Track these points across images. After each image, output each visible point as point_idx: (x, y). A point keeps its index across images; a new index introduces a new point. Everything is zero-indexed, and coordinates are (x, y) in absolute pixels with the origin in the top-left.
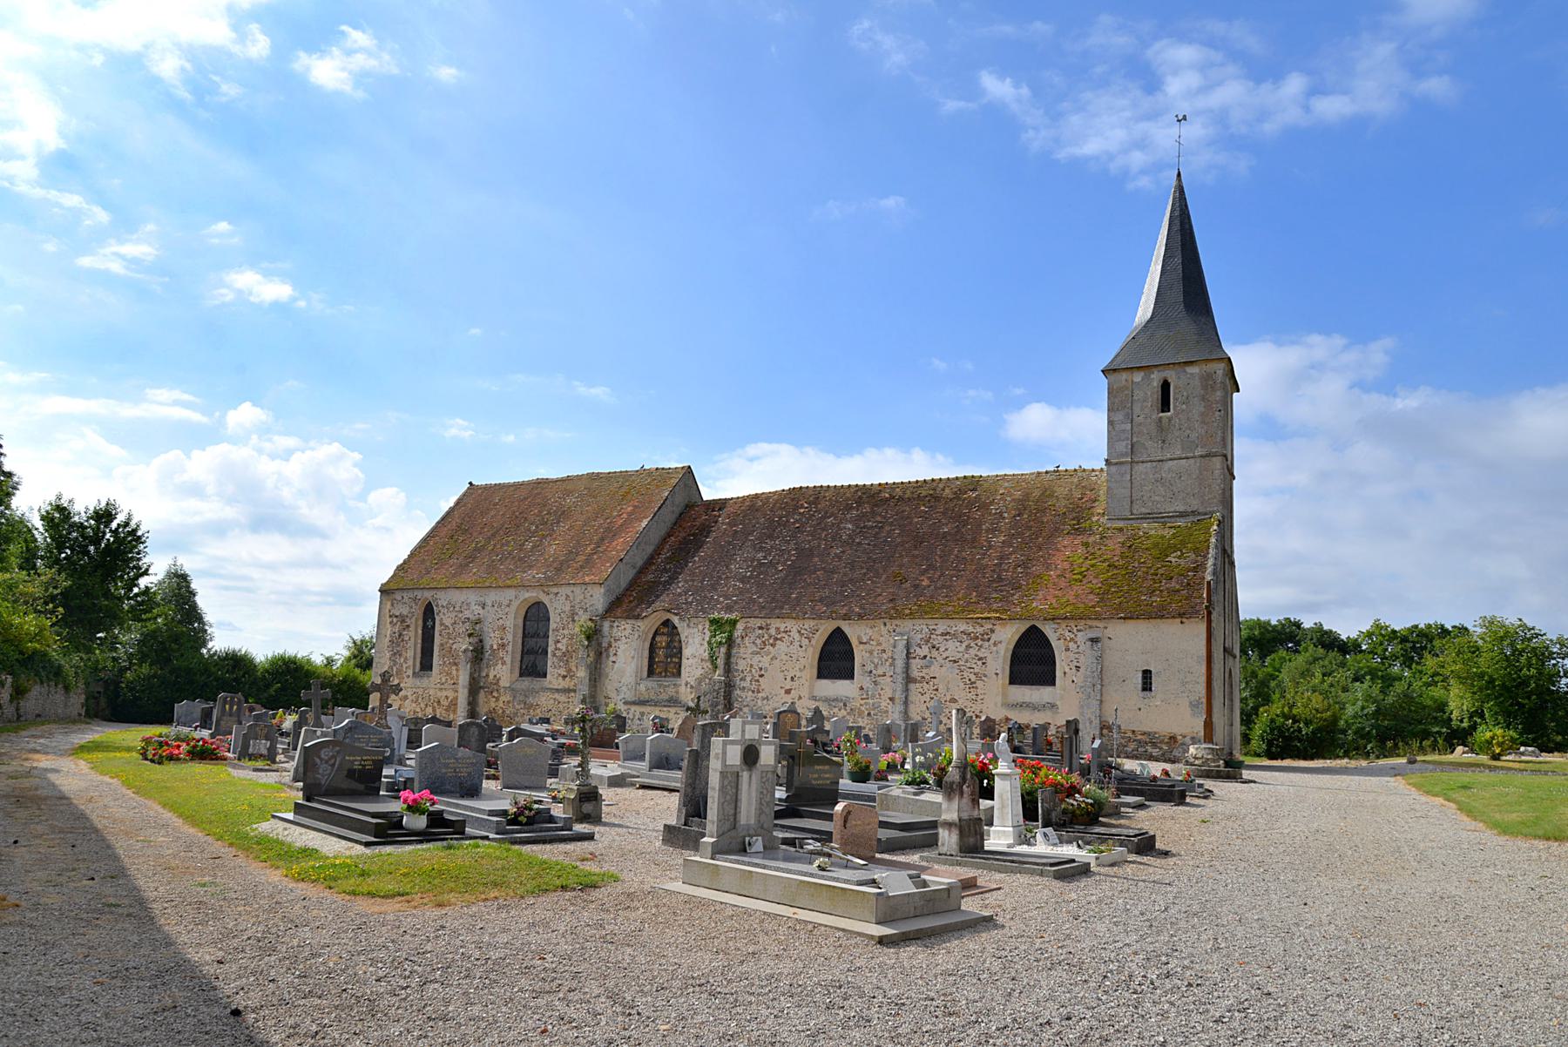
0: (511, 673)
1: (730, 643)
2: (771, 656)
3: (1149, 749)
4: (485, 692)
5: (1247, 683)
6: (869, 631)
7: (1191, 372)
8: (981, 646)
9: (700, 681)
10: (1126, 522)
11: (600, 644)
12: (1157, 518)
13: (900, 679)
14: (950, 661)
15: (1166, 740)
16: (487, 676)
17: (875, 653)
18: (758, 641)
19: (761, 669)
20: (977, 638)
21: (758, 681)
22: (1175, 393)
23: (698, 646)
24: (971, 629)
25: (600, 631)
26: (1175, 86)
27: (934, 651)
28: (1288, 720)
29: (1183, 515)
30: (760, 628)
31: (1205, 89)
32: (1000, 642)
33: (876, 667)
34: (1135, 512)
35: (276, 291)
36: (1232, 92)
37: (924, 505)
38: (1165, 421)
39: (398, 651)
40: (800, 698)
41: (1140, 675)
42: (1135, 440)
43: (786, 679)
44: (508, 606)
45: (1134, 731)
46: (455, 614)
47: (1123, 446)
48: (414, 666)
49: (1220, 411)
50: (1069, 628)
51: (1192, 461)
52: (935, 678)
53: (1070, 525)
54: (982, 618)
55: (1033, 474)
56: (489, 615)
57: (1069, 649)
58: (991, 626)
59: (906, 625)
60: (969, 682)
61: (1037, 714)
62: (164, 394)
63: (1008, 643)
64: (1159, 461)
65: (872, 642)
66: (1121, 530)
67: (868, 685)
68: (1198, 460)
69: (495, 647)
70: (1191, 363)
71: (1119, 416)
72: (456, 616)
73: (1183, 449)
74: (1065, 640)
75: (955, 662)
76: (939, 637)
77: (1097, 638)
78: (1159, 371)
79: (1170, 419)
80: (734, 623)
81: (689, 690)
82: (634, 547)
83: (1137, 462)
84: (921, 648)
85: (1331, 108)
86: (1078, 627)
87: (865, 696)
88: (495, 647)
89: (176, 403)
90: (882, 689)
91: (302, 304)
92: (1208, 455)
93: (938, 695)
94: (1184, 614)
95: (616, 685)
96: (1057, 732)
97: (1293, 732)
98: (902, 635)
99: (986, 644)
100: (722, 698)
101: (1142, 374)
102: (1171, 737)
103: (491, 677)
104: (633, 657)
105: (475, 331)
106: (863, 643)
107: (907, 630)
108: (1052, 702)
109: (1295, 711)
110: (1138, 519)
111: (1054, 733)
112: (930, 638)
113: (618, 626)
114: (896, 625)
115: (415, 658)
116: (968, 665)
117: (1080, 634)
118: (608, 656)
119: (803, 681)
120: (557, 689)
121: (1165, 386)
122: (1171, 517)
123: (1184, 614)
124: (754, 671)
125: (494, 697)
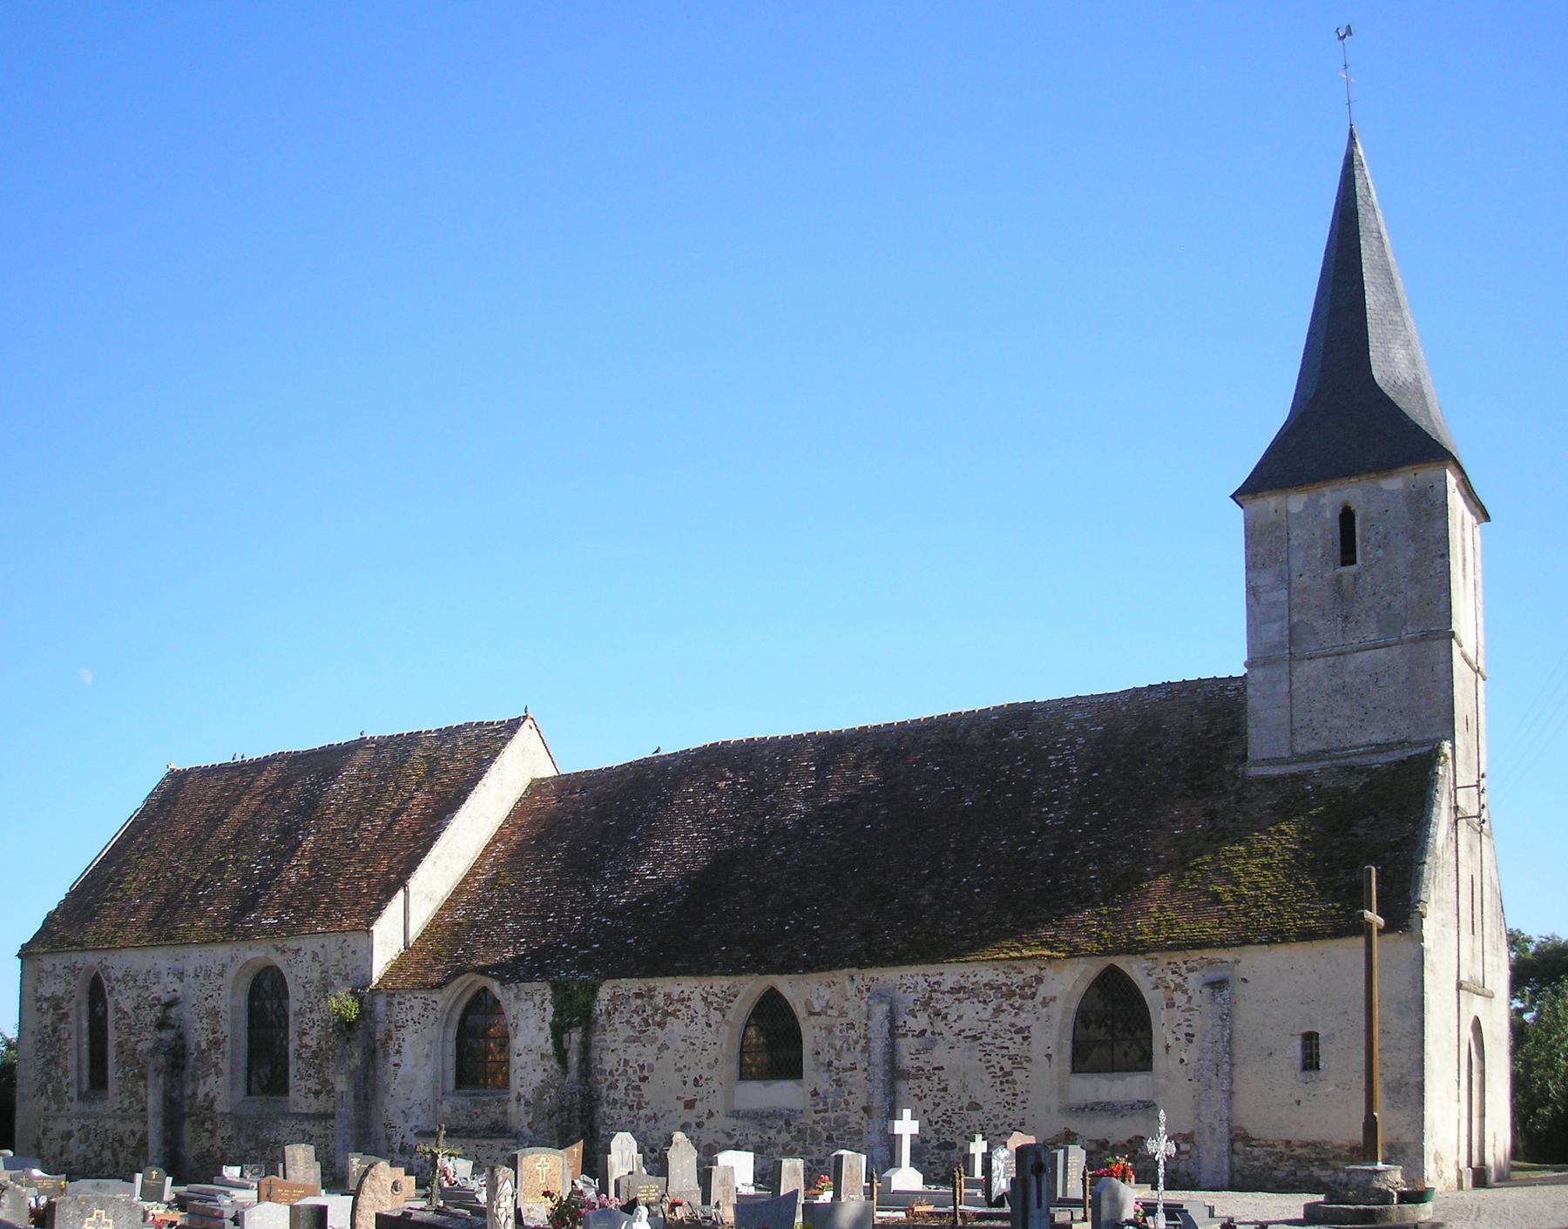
4: (193, 1122)
6: (826, 993)
13: (879, 1073)
15: (1345, 1153)
17: (837, 1030)
20: (1011, 994)
24: (1002, 979)
25: (371, 1012)
30: (638, 996)
32: (1054, 999)
33: (838, 1055)
40: (711, 1114)
41: (1298, 1042)
42: (1295, 619)
43: (685, 1083)
44: (221, 975)
45: (1288, 1143)
48: (79, 1082)
50: (1172, 966)
52: (941, 1068)
57: (1173, 1005)
64: (1338, 655)
65: (830, 1012)
69: (204, 1046)
72: (139, 996)
73: (1380, 630)
75: (975, 1038)
76: (947, 996)
79: (1356, 577)
87: (821, 1107)
88: (204, 1046)
90: (850, 1093)
93: (948, 1098)
99: (1029, 1003)
103: (201, 1097)
104: (428, 1056)
108: (1145, 1099)
112: (931, 998)
115: (79, 1068)
116: (998, 1042)
117: (1191, 976)
118: (386, 1056)
119: (714, 1085)
122: (1362, 754)
124: (630, 1071)
125: (206, 1130)
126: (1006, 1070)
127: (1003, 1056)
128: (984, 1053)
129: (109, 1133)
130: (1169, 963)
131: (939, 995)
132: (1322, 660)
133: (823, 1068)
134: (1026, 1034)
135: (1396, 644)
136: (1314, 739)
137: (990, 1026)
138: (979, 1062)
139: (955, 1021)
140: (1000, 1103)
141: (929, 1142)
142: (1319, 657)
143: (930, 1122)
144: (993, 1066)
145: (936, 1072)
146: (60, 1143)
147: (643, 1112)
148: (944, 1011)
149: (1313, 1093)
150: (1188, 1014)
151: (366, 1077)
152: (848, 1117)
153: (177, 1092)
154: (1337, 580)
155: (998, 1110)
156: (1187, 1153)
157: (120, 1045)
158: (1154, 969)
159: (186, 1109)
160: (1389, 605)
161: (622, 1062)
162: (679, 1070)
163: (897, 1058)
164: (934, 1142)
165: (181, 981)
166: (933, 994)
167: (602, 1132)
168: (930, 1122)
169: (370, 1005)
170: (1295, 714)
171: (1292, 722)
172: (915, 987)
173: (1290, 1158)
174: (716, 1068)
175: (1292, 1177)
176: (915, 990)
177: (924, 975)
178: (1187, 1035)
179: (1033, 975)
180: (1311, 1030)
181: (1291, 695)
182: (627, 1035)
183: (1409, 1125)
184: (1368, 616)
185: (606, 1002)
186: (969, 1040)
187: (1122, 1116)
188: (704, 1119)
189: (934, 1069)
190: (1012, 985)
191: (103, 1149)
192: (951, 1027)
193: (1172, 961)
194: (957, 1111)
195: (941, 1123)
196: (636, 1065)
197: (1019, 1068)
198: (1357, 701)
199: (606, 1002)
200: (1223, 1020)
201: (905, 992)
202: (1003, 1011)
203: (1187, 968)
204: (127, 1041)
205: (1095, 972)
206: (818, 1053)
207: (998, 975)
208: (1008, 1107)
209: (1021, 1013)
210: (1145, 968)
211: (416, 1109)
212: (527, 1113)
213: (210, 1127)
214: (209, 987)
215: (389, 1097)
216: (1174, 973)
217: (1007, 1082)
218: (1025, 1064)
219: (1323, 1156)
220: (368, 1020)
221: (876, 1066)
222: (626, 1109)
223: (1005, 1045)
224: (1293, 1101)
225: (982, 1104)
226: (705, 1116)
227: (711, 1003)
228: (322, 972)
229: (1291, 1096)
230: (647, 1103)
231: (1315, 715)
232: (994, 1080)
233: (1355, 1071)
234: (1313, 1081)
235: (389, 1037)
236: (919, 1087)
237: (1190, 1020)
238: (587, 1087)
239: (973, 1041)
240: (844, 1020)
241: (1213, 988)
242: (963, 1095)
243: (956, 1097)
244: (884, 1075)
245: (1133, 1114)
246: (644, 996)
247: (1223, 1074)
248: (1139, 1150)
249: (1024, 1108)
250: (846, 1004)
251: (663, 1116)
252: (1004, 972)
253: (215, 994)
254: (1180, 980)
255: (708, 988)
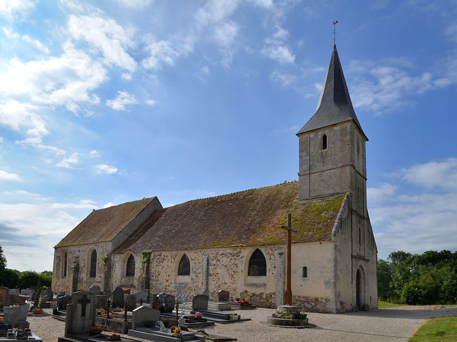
0: (86, 276)
1: (148, 261)
2: (162, 266)
3: (306, 304)
4: (80, 283)
5: (401, 274)
6: (195, 255)
7: (336, 129)
8: (236, 259)
9: (140, 277)
10: (307, 201)
11: (110, 264)
12: (321, 197)
13: (205, 274)
14: (224, 266)
15: (314, 300)
16: (80, 277)
17: (197, 264)
18: (158, 261)
19: (159, 272)
20: (234, 255)
21: (158, 277)
22: (328, 140)
23: (139, 263)
24: (232, 252)
25: (110, 259)
26: (383, 82)
27: (218, 262)
28: (415, 288)
29: (332, 195)
30: (159, 255)
31: (396, 81)
32: (243, 257)
33: (197, 269)
34: (311, 196)
35: (113, 170)
36: (405, 81)
37: (231, 203)
38: (324, 153)
39: (58, 269)
40: (171, 283)
41: (302, 269)
42: (311, 163)
43: (167, 276)
44: (86, 251)
45: (299, 296)
46: (72, 255)
47: (306, 167)
48: (62, 274)
49: (349, 145)
50: (271, 249)
51: (336, 170)
52: (218, 274)
53: (284, 204)
54: (235, 247)
55: (275, 186)
56: (81, 255)
57: (271, 259)
58: (240, 250)
59: (208, 251)
60: (231, 275)
61: (258, 289)
62: (86, 201)
63: (247, 257)
64: (321, 172)
65: (196, 259)
66: (304, 204)
67: (194, 277)
68: (339, 169)
69: (82, 267)
70: (335, 125)
71: (304, 154)
72: (72, 256)
73: (332, 165)
74: (270, 254)
75: (226, 266)
76: (220, 256)
77: (282, 253)
78: (321, 131)
79: (326, 152)
80: (150, 254)
81: (136, 281)
82: (128, 227)
83: (312, 173)
84: (213, 261)
85: (442, 83)
86: (275, 248)
87: (193, 282)
88: (82, 267)
89: (89, 204)
90: (199, 279)
91: (120, 173)
92: (343, 166)
93: (220, 281)
94: (321, 239)
95: (115, 279)
96: (266, 297)
97: (418, 293)
98: (206, 255)
99: (238, 258)
100: (145, 284)
101: (314, 133)
102: (316, 299)
103: (81, 278)
104: (120, 269)
105: (172, 178)
106: (192, 260)
107: (208, 253)
108: (265, 283)
109: (418, 284)
110: (312, 199)
111: (265, 297)
112: (217, 256)
113: (116, 257)
114: (205, 252)
115: (62, 271)
116: (231, 267)
117: (276, 251)
118: (113, 269)
119: (172, 276)
120: (98, 282)
121: (325, 137)
122: (327, 196)
123: (321, 239)
124: (156, 273)
125: (82, 285)
126: (232, 274)
127: (232, 271)
128: (227, 270)
129: (66, 285)
130: (270, 248)
131: (218, 256)
132: (317, 173)
133: (194, 273)
134: (237, 266)
135: (336, 168)
136: (315, 193)
137: (229, 263)
138: (226, 272)
139: (221, 262)
140: (231, 283)
141: (215, 292)
142: (316, 173)
143: (216, 287)
144: (230, 273)
145: (217, 274)
146: (58, 287)
147: (158, 282)
148: (219, 259)
149: (305, 283)
150: (274, 261)
151: (108, 273)
152: (199, 285)
153: (77, 277)
154: (322, 153)
155: (231, 284)
156: (274, 298)
157: (69, 266)
158: (266, 249)
159: (79, 280)
160: (335, 158)
161: (155, 271)
162: (166, 273)
163: (209, 271)
164: (216, 292)
165: (79, 253)
166: (217, 255)
167: (150, 287)
168: (216, 287)
169: (110, 257)
170: (310, 187)
171: (310, 189)
172: (213, 254)
173: (300, 301)
174: (173, 272)
175: (300, 306)
176: (213, 255)
177: (215, 251)
178: (274, 267)
179: (239, 251)
180: (305, 266)
181: (309, 182)
182: (156, 264)
183: (331, 293)
184: (329, 161)
185: (153, 257)
186: (224, 267)
187: (259, 287)
188: (170, 284)
189: (217, 274)
190: (234, 253)
191: (65, 289)
192: (221, 263)
193: (271, 247)
194: (221, 284)
195: (218, 287)
196: (157, 271)
197: (235, 274)
198: (326, 183)
199: (153, 257)
200: (282, 263)
201: (211, 255)
202: (232, 260)
203: (274, 249)
204: (70, 265)
205: (355, 282)
206: (193, 269)
207: (231, 251)
208: (233, 284)
209: (236, 260)
210: (265, 249)
211: (117, 281)
212: (137, 282)
213: (82, 284)
214: (84, 254)
215: (113, 278)
216: (271, 250)
217: (233, 277)
218: (237, 273)
219: (308, 301)
220: (109, 261)
221: (204, 272)
222: (155, 281)
223: (232, 268)
224: (300, 285)
225: (227, 283)
226: (170, 284)
227: (172, 257)
228: (103, 250)
229: (300, 284)
230: (159, 280)
231: (316, 187)
232: (230, 277)
233: (316, 278)
234: (306, 280)
235: (113, 265)
236: (214, 278)
237: (275, 263)
238: (148, 276)
239: (225, 267)
240: (198, 261)
241: (280, 254)
242: (223, 280)
243: (221, 281)
244: (206, 275)
245: (261, 287)
246: (160, 255)
247: (282, 277)
248: (262, 296)
249: (236, 284)
250: (199, 257)
251: (162, 283)
252: (232, 250)
253: (85, 255)
254: (272, 252)
255: (172, 254)
